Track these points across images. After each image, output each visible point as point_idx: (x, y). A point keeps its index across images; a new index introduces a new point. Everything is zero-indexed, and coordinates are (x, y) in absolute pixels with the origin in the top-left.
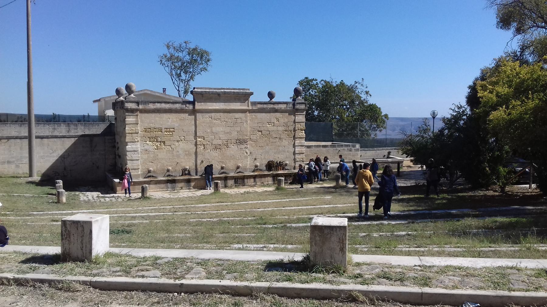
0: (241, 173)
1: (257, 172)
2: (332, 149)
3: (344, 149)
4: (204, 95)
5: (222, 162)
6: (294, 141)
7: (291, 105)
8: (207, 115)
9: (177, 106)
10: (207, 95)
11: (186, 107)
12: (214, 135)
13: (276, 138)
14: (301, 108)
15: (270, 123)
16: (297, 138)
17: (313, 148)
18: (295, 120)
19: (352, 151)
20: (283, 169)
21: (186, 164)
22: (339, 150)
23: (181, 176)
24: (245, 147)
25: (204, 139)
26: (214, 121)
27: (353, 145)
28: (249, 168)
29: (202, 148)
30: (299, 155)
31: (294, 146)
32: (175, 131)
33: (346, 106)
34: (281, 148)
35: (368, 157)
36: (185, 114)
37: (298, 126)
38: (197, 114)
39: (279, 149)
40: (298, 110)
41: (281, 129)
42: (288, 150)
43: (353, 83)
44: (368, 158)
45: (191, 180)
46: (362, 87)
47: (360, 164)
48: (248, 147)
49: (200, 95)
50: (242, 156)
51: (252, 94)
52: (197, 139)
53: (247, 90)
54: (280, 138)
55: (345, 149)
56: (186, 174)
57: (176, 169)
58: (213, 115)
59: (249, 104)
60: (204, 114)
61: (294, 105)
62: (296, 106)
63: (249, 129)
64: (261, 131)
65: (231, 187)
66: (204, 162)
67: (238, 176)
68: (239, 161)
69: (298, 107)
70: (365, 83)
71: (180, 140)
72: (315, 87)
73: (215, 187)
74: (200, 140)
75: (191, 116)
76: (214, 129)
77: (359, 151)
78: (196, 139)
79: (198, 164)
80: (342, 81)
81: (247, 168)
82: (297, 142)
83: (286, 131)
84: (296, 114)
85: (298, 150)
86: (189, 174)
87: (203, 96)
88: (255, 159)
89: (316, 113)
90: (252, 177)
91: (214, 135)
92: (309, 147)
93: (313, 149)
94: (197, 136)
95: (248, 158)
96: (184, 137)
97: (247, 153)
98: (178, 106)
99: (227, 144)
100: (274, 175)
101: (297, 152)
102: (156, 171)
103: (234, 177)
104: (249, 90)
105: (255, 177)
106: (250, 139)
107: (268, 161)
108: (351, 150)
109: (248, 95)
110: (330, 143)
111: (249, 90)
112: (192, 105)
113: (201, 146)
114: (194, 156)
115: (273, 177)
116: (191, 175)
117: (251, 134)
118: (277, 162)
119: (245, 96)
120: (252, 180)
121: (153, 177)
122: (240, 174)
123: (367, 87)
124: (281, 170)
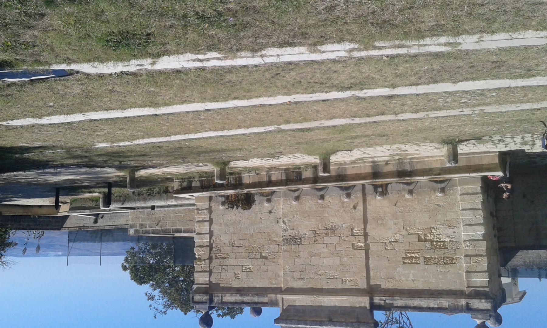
5: (322, 206)
8: (348, 285)
9: (401, 301)
13: (238, 247)
15: (249, 270)
16: (207, 246)
18: (210, 275)
20: (227, 197)
23: (388, 184)
24: (287, 232)
25: (353, 244)
26: (336, 275)
29: (356, 230)
30: (205, 220)
31: (211, 234)
32: (401, 259)
34: (232, 229)
35: (124, 215)
37: (205, 265)
41: (232, 262)
43: (169, 311)
44: (125, 214)
49: (362, 321)
50: (291, 217)
51: (277, 321)
52: (364, 245)
56: (381, 186)
57: (398, 195)
58: (340, 286)
59: (281, 304)
63: (281, 261)
64: (262, 257)
65: (307, 166)
66: (351, 207)
68: (295, 210)
69: (205, 298)
70: (152, 312)
71: (393, 243)
74: (359, 244)
75: (375, 284)
78: (367, 246)
79: (362, 204)
82: (206, 240)
83: (224, 258)
84: (208, 286)
85: (206, 228)
86: (376, 187)
87: (357, 318)
88: (270, 212)
90: (274, 183)
91: (336, 252)
94: (364, 251)
95: (281, 213)
97: (284, 222)
101: (207, 224)
102: (431, 190)
103: (301, 182)
105: (270, 183)
106: (278, 245)
107: (251, 210)
108: (141, 225)
110: (177, 235)
113: (357, 233)
114: (369, 217)
116: (373, 185)
117: (277, 252)
118: (237, 207)
120: (274, 178)
121: (437, 182)
122: (294, 187)
123: (150, 306)
124: (232, 195)
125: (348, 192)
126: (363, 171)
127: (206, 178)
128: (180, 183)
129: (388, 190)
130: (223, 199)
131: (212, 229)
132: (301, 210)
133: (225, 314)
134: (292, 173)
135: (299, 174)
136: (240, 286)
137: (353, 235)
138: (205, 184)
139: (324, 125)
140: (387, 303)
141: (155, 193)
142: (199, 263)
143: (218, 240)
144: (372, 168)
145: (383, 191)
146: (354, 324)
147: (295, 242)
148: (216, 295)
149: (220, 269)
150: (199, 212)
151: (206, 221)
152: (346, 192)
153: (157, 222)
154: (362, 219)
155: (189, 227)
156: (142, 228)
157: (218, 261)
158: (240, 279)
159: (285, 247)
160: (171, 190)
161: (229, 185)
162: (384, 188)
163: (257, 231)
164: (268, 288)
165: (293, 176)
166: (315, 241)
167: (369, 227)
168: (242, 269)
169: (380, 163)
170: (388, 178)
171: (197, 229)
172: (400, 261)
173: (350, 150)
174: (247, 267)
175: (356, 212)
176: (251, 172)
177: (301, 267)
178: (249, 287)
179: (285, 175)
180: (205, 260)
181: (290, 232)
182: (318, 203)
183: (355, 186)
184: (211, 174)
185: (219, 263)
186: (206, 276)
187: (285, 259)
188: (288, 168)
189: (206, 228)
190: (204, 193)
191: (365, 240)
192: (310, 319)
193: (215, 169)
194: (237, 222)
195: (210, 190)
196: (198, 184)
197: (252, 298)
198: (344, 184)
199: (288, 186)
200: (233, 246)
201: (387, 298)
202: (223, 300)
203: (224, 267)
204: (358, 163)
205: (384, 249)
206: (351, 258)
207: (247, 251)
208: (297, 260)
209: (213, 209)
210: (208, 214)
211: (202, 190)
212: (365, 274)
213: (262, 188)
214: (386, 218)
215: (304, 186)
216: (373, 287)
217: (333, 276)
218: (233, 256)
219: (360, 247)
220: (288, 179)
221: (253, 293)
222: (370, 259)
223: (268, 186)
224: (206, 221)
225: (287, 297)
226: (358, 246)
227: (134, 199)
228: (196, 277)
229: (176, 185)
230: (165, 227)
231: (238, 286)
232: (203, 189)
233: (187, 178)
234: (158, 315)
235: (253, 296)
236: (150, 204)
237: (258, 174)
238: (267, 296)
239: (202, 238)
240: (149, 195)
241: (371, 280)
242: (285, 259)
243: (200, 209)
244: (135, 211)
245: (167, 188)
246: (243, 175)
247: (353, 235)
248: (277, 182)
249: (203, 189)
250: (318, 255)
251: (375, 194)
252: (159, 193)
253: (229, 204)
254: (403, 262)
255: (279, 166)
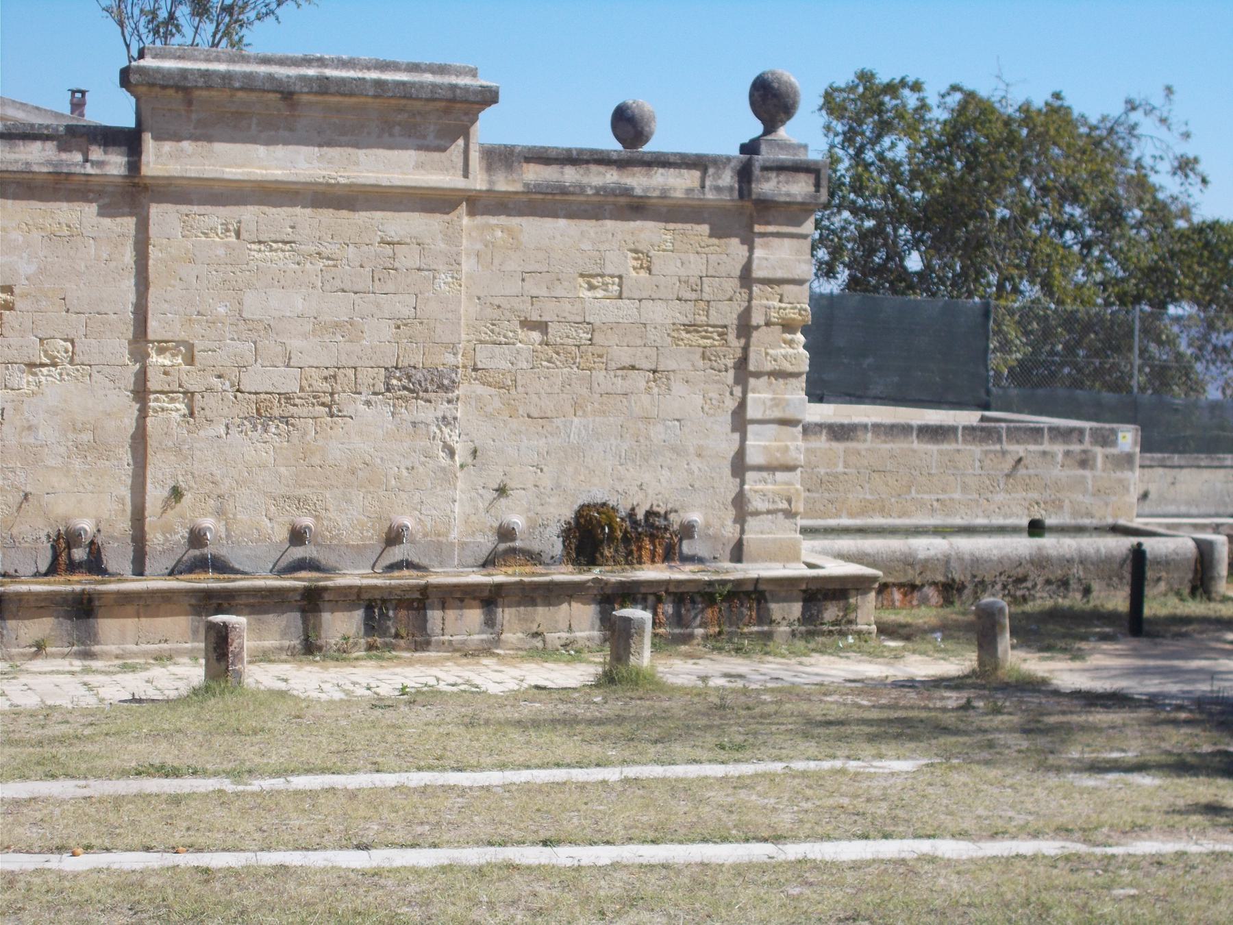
0: (414, 573)
1: (510, 571)
2: (977, 450)
3: (1044, 453)
4: (198, 93)
5: (301, 502)
6: (738, 391)
7: (727, 178)
8: (216, 216)
9: (30, 158)
10: (213, 93)
11: (86, 160)
12: (254, 336)
13: (633, 368)
14: (788, 195)
15: (594, 281)
16: (758, 375)
17: (865, 441)
18: (747, 270)
19: (1093, 468)
20: (670, 554)
21: (80, 502)
22: (1020, 460)
23: (46, 574)
24: (440, 414)
25: (190, 360)
26: (258, 254)
27: (1097, 429)
28: (463, 545)
29: (178, 410)
30: (765, 474)
31: (740, 421)
32: (18, 305)
33: (1077, 228)
34: (657, 433)
35: (1188, 503)
36: (77, 206)
37: (766, 303)
38: (155, 210)
39: (648, 438)
40: (767, 209)
41: (662, 314)
42: (701, 442)
43: (1115, 109)
44: (1183, 509)
45: (97, 603)
46: (1162, 132)
47: (1134, 540)
48: (459, 415)
49: (171, 92)
50: (421, 469)
51: (489, 97)
52: (148, 355)
53: (459, 72)
54: (655, 372)
55: (1053, 456)
56: (73, 567)
57: (15, 531)
58: (249, 214)
59: (475, 156)
60: (195, 209)
61: (745, 174)
62: (758, 181)
63: (467, 309)
64: (542, 327)
65: (342, 655)
66: (188, 498)
67: (391, 589)
68: (404, 495)
69: (768, 186)
70: (1178, 113)
71: (45, 360)
72: (914, 122)
73: (213, 656)
74: (167, 362)
75: (119, 220)
76: (250, 298)
77: (1132, 469)
78: (139, 355)
79: (148, 505)
80: (1057, 96)
81: (452, 544)
82: (760, 399)
83: (691, 327)
84: (758, 228)
85: (760, 444)
86: (95, 564)
87: (189, 103)
88: (502, 491)
89: (914, 262)
90: (474, 598)
91: (254, 336)
92: (840, 432)
93: (867, 445)
94: (151, 336)
95: (459, 484)
96: (69, 345)
97: (452, 453)
98: (37, 155)
99: (332, 394)
100: (609, 591)
101: (753, 457)
103: (365, 596)
104: (475, 76)
105: (490, 598)
106: (475, 369)
107: (580, 502)
108: (1085, 462)
109: (466, 101)
110: (970, 417)
111: (475, 76)
112: (122, 154)
113: (172, 400)
114: (126, 456)
115: (600, 603)
116: (104, 572)
117: (481, 342)
118: (632, 514)
119: (447, 111)
120: (474, 615)
121: (410, 565)
122: (408, 578)
123: (1186, 135)
124: (653, 561)
125: (197, 552)
126: (130, 623)
127: (746, 630)
128: (852, 616)
129: (49, 554)
130: (687, 547)
131: (737, 436)
132: (381, 493)
133: (891, 89)
134: (403, 632)
135: (371, 626)
136: (632, 224)
137: (189, 395)
138: (750, 609)
139: (77, 782)
140: (80, 150)
141: (998, 587)
142: (792, 314)
143: (714, 395)
144: (96, 635)
145: (69, 547)
146: (201, 82)
147: (409, 377)
148: (726, 196)
149: (706, 288)
150: (785, 505)
151: (759, 468)
152: (205, 550)
153: (1022, 471)
154: (150, 451)
155: (889, 446)
156: (1084, 452)
157: (715, 318)
158: (631, 250)
159: (450, 359)
160: (931, 592)
161: (651, 599)
162: (63, 558)
163: (558, 422)
164: (521, 214)
165: (397, 619)
166: (334, 377)
167: (126, 420)
168: (620, 285)
169: (67, 650)
170: (38, 594)
171: (795, 439)
172: (25, 296)
173: (134, 700)
174: (600, 293)
175: (174, 476)
176: (565, 646)
177: (390, 287)
178: (597, 219)
179: (429, 625)
180: (768, 324)
181: (426, 412)
182: (316, 517)
183: (171, 573)
184: (662, 644)
185: (712, 312)
186: (765, 263)
187: (450, 315)
188: (416, 650)
189: (760, 444)
190: (753, 574)
191: (145, 373)
192: (363, 100)
193: (644, 657)
194: (633, 461)
195: (729, 587)
196: (776, 610)
197: (585, 180)
198: (208, 581)
199: (417, 586)
200: (655, 372)
201: (78, 170)
202: (697, 174)
203: (694, 296)
204: (145, 654)
205: (76, 340)
206: (199, 313)
207: (599, 350)
208: (407, 312)
209: (731, 513)
210: (749, 494)
211: (762, 587)
212: (153, 253)
213: (521, 583)
214: (62, 450)
215: (366, 582)
216: (127, 210)
217: (271, 250)
218: (652, 335)
219: (166, 349)
220: (418, 609)
221: (582, 198)
222: (130, 308)
223: (499, 587)
224: (759, 468)
225: (448, 178)
226: (173, 355)
227: (1085, 569)
228: (805, 262)
229: (867, 610)
230: (986, 453)
231: (639, 223)
232: (755, 591)
233: (822, 633)
234: (1157, 100)
235: (582, 188)
236: (1049, 543)
237: (536, 635)
238: (526, 185)
239: (777, 405)
240: (1023, 579)
241: (133, 232)
242: (450, 315)
243: (780, 515)
244: (1110, 521)
245: (948, 602)
246: (596, 633)
247: (189, 395)
248: (462, 600)
249: (755, 591)
250: (322, 327)
251: (99, 541)
252: (982, 582)
253: (666, 529)
254: (12, 293)
255: (448, 659)
